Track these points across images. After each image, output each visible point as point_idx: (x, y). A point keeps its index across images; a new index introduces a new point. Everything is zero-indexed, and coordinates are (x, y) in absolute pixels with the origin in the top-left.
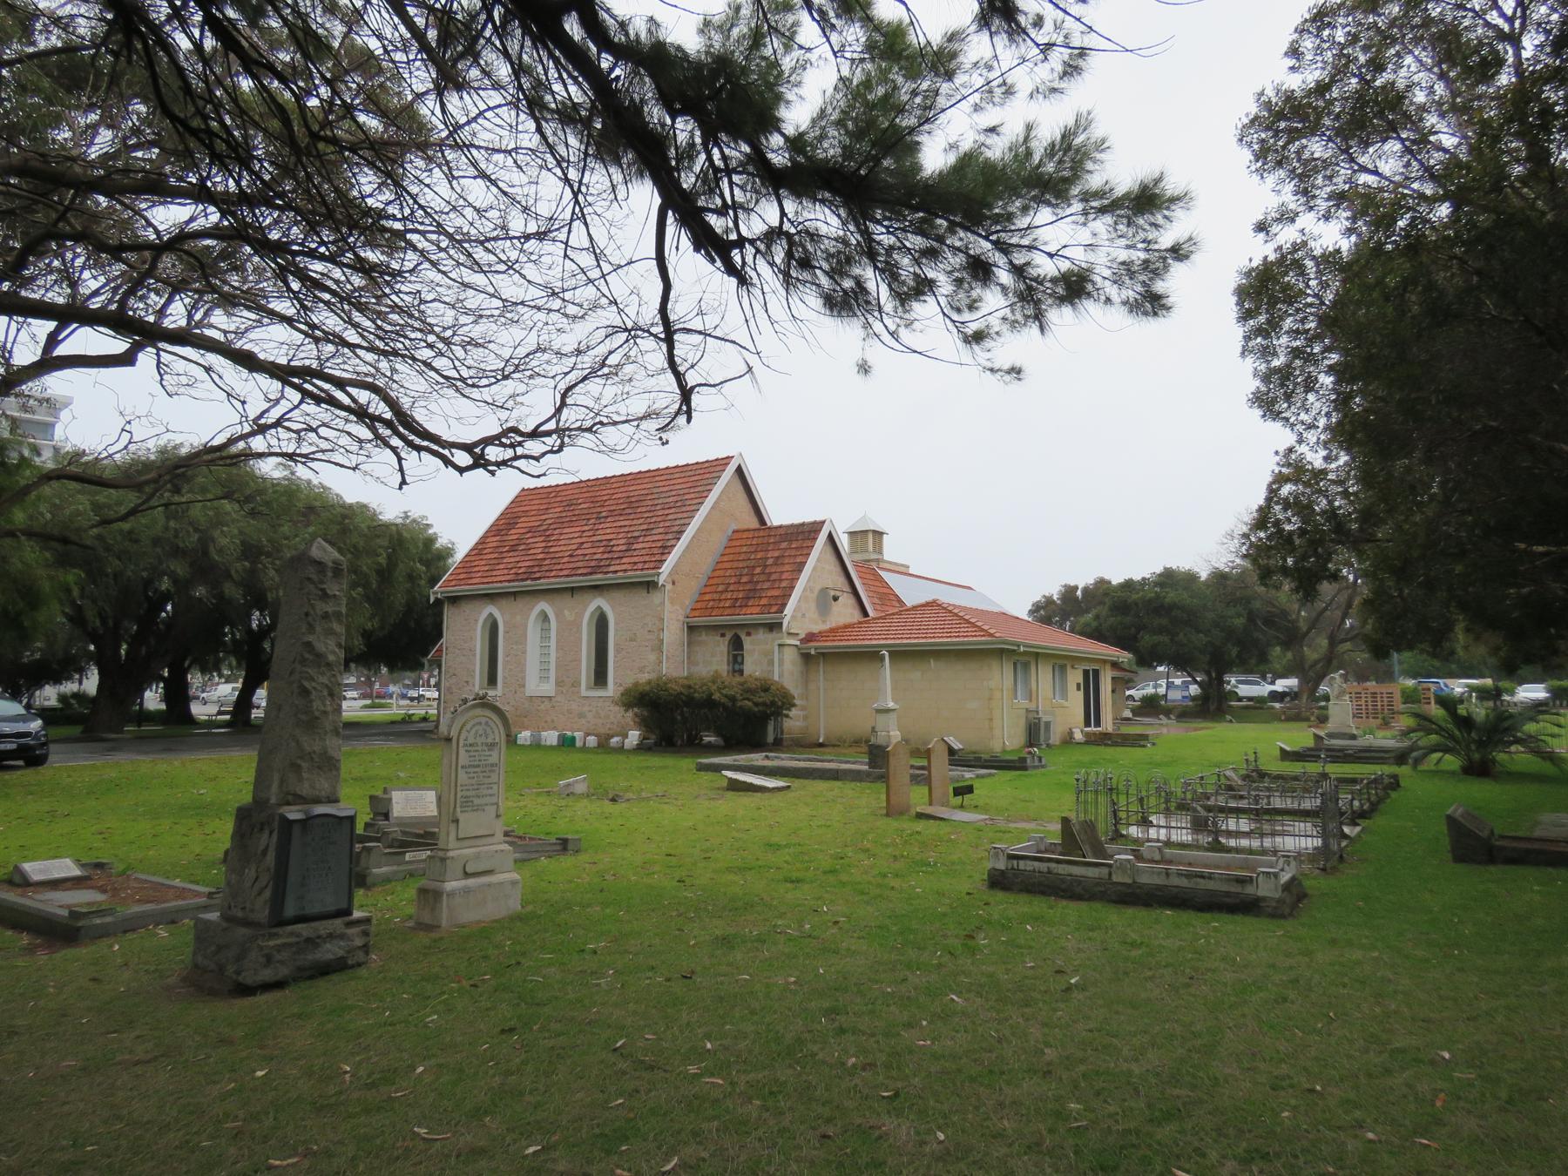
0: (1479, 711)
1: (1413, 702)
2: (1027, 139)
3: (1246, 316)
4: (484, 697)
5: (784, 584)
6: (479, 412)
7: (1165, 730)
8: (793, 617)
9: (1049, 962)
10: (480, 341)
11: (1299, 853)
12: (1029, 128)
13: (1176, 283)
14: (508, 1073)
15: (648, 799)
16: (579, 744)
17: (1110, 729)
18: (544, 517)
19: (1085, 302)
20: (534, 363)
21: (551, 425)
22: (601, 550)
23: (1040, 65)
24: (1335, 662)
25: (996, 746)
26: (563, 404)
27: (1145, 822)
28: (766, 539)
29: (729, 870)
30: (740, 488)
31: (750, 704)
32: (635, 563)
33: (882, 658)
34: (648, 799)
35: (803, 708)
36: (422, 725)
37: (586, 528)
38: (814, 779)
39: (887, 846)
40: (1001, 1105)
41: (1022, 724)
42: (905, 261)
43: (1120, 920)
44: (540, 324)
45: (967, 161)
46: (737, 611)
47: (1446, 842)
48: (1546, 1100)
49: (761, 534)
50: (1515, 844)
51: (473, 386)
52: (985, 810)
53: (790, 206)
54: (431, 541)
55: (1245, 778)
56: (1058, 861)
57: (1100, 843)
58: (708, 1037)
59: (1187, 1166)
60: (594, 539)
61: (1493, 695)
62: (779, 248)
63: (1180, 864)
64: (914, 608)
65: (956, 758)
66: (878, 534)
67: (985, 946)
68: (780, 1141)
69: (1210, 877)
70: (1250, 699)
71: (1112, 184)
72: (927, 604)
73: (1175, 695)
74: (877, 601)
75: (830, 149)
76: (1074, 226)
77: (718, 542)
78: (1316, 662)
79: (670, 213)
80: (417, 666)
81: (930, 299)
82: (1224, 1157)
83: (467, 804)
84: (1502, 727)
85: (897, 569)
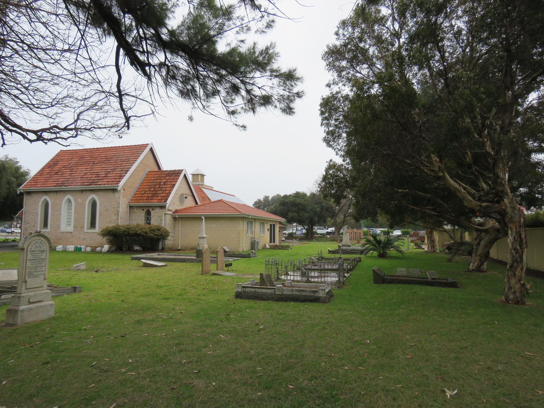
0: (383, 238)
1: (366, 235)
2: (254, 47)
3: (322, 113)
4: (39, 232)
5: (167, 192)
6: (40, 118)
7: (295, 244)
8: (170, 204)
9: (254, 322)
10: (42, 90)
11: (332, 283)
12: (255, 44)
13: (297, 104)
14: (46, 379)
15: (111, 271)
16: (83, 250)
17: (278, 244)
18: (70, 162)
19: (270, 106)
20: (65, 102)
21: (73, 126)
22: (94, 176)
23: (259, 22)
24: (345, 223)
25: (241, 250)
26: (78, 118)
27: (287, 274)
28: (161, 175)
29: (142, 296)
30: (151, 156)
31: (153, 235)
32: (109, 182)
33: (202, 219)
34: (111, 271)
35: (173, 237)
36: (13, 243)
37: (88, 167)
38: (177, 262)
39: (201, 285)
40: (235, 371)
41: (249, 242)
42: (210, 82)
43: (277, 306)
44: (69, 86)
45: (233, 51)
46: (149, 201)
47: (372, 277)
48: (393, 352)
49: (159, 173)
50: (390, 278)
51: (38, 108)
52: (236, 271)
53: (169, 56)
54: (18, 168)
55: (318, 259)
56: (258, 288)
57: (272, 282)
58: (130, 357)
59: (293, 384)
60: (91, 171)
61: (387, 233)
62: (164, 70)
63: (297, 287)
64: (214, 202)
65: (226, 254)
66: (203, 176)
67: (233, 318)
68: (156, 392)
69: (305, 291)
70: (321, 234)
71: (281, 68)
72: (219, 201)
73: (298, 233)
74: (201, 199)
75: (184, 38)
76: (267, 80)
77: (142, 175)
78: (340, 223)
79: (121, 49)
80: (11, 219)
81: (217, 97)
82: (304, 380)
83: (31, 275)
84: (388, 243)
85: (207, 187)
